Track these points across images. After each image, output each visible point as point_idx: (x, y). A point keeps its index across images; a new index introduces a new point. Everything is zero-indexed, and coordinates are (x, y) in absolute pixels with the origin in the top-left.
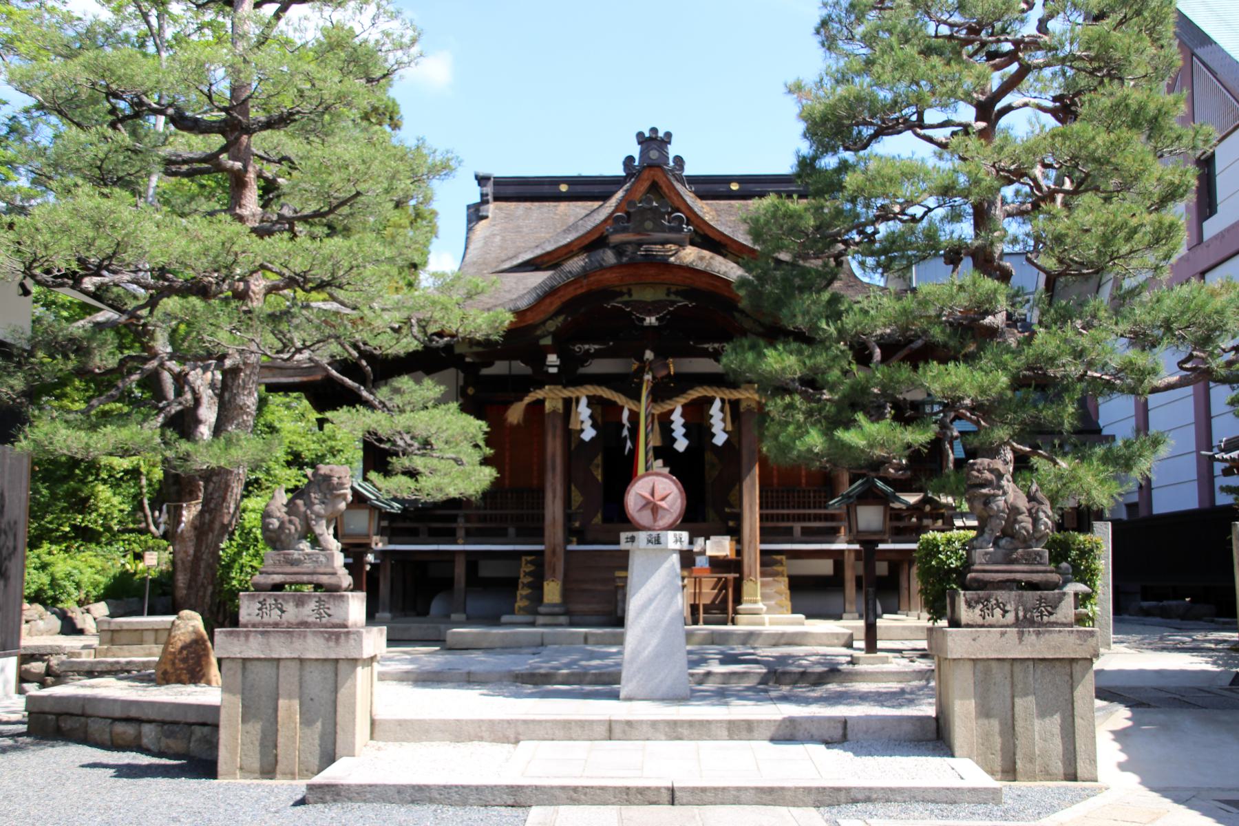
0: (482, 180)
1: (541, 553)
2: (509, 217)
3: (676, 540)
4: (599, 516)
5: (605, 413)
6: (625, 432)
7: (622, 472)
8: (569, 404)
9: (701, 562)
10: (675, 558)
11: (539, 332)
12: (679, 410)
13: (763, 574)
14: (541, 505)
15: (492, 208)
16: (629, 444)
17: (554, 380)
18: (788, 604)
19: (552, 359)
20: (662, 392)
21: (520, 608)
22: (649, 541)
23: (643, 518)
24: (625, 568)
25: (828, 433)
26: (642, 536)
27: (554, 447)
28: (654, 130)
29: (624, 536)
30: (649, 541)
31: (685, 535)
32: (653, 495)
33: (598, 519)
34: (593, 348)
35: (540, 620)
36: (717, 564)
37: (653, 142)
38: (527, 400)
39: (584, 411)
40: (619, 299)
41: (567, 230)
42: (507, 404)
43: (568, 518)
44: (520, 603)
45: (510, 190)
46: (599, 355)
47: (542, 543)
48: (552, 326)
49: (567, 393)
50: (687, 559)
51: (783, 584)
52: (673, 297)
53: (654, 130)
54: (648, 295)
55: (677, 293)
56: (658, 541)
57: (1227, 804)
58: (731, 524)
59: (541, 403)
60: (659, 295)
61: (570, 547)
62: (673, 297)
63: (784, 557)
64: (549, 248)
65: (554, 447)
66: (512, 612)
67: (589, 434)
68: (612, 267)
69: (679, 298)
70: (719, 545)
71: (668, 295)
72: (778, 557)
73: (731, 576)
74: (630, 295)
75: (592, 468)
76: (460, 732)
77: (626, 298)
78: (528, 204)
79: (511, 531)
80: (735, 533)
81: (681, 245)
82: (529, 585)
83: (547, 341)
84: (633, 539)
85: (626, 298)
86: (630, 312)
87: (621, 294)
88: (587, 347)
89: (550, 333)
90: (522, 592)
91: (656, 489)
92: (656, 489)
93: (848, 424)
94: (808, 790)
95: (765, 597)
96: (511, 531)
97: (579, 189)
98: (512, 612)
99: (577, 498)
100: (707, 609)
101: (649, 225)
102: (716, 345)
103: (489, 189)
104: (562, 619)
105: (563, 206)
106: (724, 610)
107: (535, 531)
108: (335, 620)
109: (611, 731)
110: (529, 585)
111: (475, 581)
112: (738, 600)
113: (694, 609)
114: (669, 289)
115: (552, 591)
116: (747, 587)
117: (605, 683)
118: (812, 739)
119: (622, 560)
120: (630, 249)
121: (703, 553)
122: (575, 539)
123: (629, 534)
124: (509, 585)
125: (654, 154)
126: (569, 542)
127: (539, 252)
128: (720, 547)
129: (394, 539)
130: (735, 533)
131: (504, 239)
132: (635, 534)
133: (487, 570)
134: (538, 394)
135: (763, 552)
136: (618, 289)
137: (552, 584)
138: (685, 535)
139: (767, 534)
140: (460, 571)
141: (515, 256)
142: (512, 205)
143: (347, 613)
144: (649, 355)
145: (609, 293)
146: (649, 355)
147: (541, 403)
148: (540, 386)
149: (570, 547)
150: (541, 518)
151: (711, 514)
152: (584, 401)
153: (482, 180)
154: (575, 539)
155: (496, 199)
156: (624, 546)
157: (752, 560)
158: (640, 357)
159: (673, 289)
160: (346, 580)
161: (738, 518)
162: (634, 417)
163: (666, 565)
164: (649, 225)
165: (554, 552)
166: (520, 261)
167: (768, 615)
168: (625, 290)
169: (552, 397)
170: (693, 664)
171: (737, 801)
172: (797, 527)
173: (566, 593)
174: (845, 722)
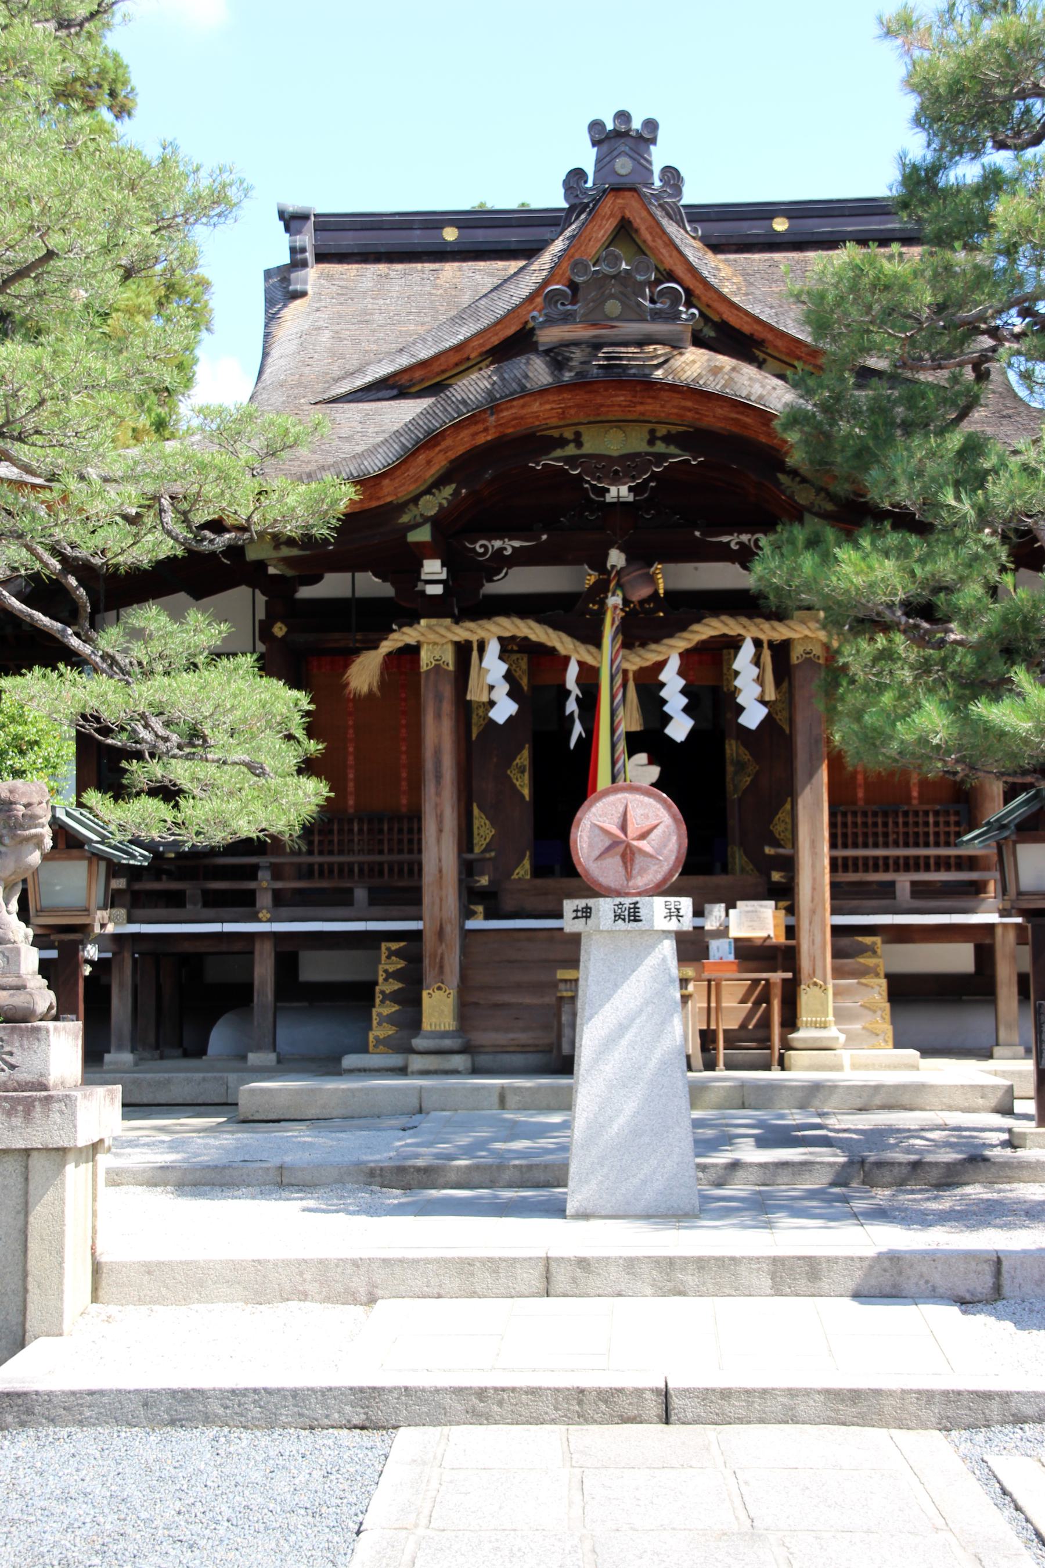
0: (292, 220)
2: (346, 294)
3: (668, 914)
4: (527, 863)
5: (535, 673)
6: (571, 706)
7: (566, 782)
8: (464, 652)
9: (720, 950)
10: (668, 947)
11: (405, 519)
12: (674, 663)
13: (838, 973)
14: (415, 845)
15: (313, 276)
16: (578, 729)
17: (436, 608)
18: (887, 1028)
19: (433, 568)
20: (639, 629)
21: (378, 1041)
22: (618, 917)
24: (574, 963)
25: (957, 707)
26: (604, 907)
27: (438, 735)
29: (569, 906)
30: (618, 917)
31: (686, 904)
32: (624, 828)
33: (524, 870)
34: (509, 545)
35: (417, 1062)
36: (750, 954)
38: (387, 646)
39: (493, 668)
40: (558, 453)
41: (459, 319)
42: (348, 655)
43: (468, 868)
44: (379, 1031)
45: (348, 241)
46: (521, 558)
47: (419, 918)
48: (430, 506)
49: (463, 632)
50: (692, 947)
51: (877, 991)
52: (660, 447)
54: (613, 443)
55: (668, 439)
56: (634, 916)
58: (776, 876)
59: (412, 652)
60: (636, 442)
61: (471, 924)
62: (660, 447)
63: (878, 940)
64: (425, 353)
65: (438, 735)
67: (504, 710)
68: (543, 392)
69: (673, 449)
70: (755, 918)
71: (651, 442)
72: (868, 940)
73: (777, 977)
74: (579, 444)
75: (512, 773)
76: (263, 1284)
77: (571, 450)
78: (382, 268)
79: (361, 894)
80: (784, 894)
81: (676, 346)
82: (394, 997)
83: (422, 535)
84: (586, 913)
85: (571, 450)
87: (562, 442)
88: (498, 544)
89: (426, 520)
90: (382, 1009)
91: (629, 816)
92: (629, 816)
93: (998, 688)
94: (927, 1396)
95: (841, 1016)
96: (361, 894)
97: (481, 236)
98: (363, 1049)
99: (484, 830)
100: (732, 1040)
101: (613, 307)
102: (745, 538)
103: (306, 239)
104: (459, 1061)
105: (449, 270)
106: (765, 1042)
107: (403, 892)
108: (22, 1076)
109: (549, 1278)
110: (394, 997)
111: (291, 989)
112: (790, 1022)
113: (707, 1038)
114: (652, 432)
115: (438, 1009)
116: (807, 998)
117: (537, 1186)
118: (934, 1295)
119: (569, 951)
120: (577, 355)
121: (722, 932)
122: (480, 909)
123: (581, 903)
124: (357, 996)
125: (623, 166)
126: (469, 914)
127: (404, 361)
128: (756, 920)
129: (138, 912)
130: (784, 894)
131: (337, 337)
132: (591, 902)
133: (314, 969)
134: (407, 636)
135: (837, 930)
136: (555, 433)
138: (686, 904)
139: (843, 895)
140: (264, 971)
141: (360, 370)
142: (352, 270)
143: (46, 1062)
144: (616, 558)
145: (538, 442)
146: (616, 558)
147: (412, 652)
148: (411, 618)
149: (471, 924)
150: (415, 869)
151: (738, 857)
152: (493, 648)
153: (292, 220)
154: (480, 909)
155: (321, 257)
156: (569, 924)
157: (816, 946)
158: (599, 564)
159: (662, 431)
160: (44, 998)
161: (789, 865)
162: (589, 677)
163: (652, 961)
164: (613, 307)
165: (441, 934)
166: (360, 382)
167: (849, 1051)
168: (568, 434)
169: (433, 640)
170: (704, 1146)
172: (904, 881)
173: (465, 1010)
174: (997, 1262)
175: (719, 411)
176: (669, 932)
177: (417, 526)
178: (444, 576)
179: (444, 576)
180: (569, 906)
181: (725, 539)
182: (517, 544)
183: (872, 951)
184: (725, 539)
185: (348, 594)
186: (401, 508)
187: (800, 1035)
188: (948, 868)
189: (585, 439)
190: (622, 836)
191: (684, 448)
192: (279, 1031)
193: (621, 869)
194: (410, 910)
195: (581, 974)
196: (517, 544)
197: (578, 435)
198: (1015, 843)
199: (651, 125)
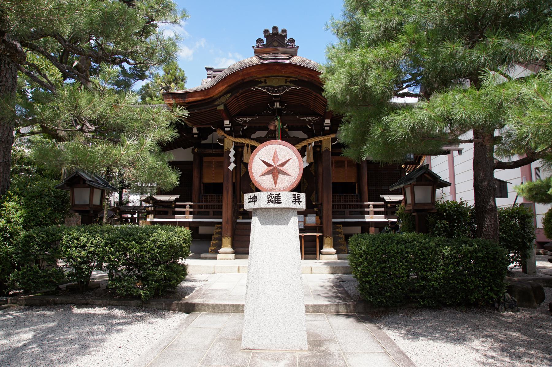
1: (220, 223)
11: (216, 103)
21: (212, 250)
22: (269, 201)
23: (265, 182)
28: (275, 28)
29: (247, 196)
30: (269, 201)
32: (268, 165)
34: (248, 119)
37: (275, 40)
40: (260, 85)
52: (288, 84)
53: (275, 28)
57: (551, 348)
61: (238, 221)
62: (288, 84)
63: (341, 225)
66: (208, 252)
69: (292, 85)
71: (286, 83)
72: (339, 225)
74: (266, 83)
77: (263, 84)
84: (255, 199)
85: (263, 84)
86: (265, 92)
87: (261, 82)
88: (245, 119)
102: (310, 118)
114: (286, 80)
122: (241, 217)
123: (252, 195)
129: (156, 216)
132: (257, 194)
133: (202, 230)
136: (259, 80)
137: (328, 238)
149: (238, 221)
154: (241, 217)
159: (289, 79)
168: (263, 80)
171: (225, 306)
172: (347, 210)
175: (305, 72)
176: (295, 209)
177: (220, 105)
178: (230, 126)
179: (230, 126)
180: (247, 196)
181: (305, 118)
182: (250, 119)
183: (340, 228)
184: (305, 118)
185: (211, 142)
186: (215, 100)
187: (324, 250)
188: (357, 205)
189: (267, 81)
190: (272, 168)
191: (296, 85)
192: (518, 198)
193: (272, 180)
194: (219, 216)
195: (298, 234)
196: (250, 119)
197: (265, 80)
198: (414, 185)
199: (284, 31)
